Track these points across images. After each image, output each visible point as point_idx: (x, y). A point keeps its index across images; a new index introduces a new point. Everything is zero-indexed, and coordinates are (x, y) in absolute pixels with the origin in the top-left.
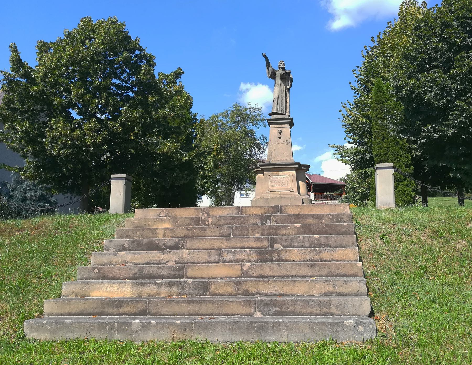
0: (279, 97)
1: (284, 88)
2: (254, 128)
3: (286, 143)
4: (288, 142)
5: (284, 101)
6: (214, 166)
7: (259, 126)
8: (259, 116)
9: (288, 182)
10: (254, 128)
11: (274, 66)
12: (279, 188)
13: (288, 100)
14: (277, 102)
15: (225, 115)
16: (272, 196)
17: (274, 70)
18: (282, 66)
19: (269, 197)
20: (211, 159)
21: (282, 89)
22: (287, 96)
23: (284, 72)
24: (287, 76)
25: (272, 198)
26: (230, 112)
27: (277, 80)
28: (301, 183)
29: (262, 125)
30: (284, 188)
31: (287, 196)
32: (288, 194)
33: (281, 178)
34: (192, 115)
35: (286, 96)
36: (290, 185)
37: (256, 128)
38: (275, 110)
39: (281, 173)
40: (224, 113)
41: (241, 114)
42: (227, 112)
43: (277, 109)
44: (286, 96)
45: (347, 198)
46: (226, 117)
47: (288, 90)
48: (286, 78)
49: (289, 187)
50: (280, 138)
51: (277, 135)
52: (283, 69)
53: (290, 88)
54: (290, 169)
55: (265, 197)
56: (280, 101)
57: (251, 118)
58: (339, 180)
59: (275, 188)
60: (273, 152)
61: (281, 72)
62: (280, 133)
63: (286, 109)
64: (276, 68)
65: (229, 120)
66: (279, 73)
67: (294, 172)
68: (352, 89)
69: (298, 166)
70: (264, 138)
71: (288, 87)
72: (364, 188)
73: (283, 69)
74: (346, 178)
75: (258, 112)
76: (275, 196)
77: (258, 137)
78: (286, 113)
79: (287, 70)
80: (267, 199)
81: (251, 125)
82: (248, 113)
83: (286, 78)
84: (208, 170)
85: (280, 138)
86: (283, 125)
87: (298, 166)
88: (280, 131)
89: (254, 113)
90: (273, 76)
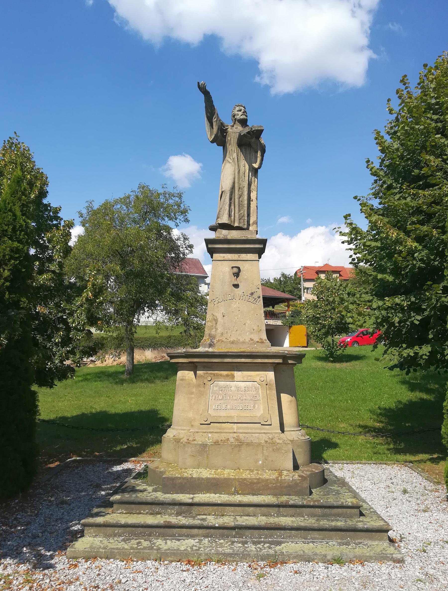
0: (233, 188)
1: (245, 166)
2: (171, 224)
3: (251, 299)
4: (255, 296)
5: (246, 198)
6: (88, 318)
7: (178, 221)
8: (179, 206)
9: (255, 400)
10: (171, 224)
11: (224, 114)
12: (235, 415)
13: (253, 195)
14: (231, 199)
15: (125, 201)
16: (216, 437)
17: (222, 124)
18: (240, 116)
19: (209, 439)
20: (82, 305)
21: (242, 169)
22: (253, 187)
23: (247, 130)
24: (253, 140)
25: (216, 443)
26: (132, 198)
27: (229, 148)
28: (285, 397)
29: (183, 219)
30: (246, 415)
31: (254, 438)
32: (257, 435)
33: (238, 389)
34: (50, 211)
35: (250, 185)
36: (262, 407)
37: (174, 223)
38: (225, 219)
39: (237, 374)
40: (124, 198)
41: (151, 202)
42: (128, 197)
43: (230, 216)
44: (250, 185)
45: (292, 316)
46: (127, 205)
47: (255, 172)
48: (251, 143)
49: (259, 414)
50: (236, 286)
51: (229, 278)
52: (244, 122)
53: (260, 167)
54: (263, 367)
55: (200, 439)
56: (237, 197)
57: (165, 209)
58: (272, 282)
59: (223, 414)
60: (220, 320)
61: (239, 128)
62: (237, 275)
63: (249, 215)
64: (228, 122)
65: (132, 210)
66: (234, 132)
67: (271, 375)
68: (372, 174)
69: (280, 361)
70: (185, 239)
71: (256, 166)
72: (332, 318)
73: (244, 122)
74: (282, 279)
75: (177, 199)
76: (223, 437)
77: (176, 237)
78: (249, 225)
79: (253, 124)
80: (204, 446)
81: (166, 219)
82: (162, 200)
83: (251, 143)
84: (76, 328)
85: (236, 286)
86: (244, 256)
87: (280, 361)
88: (236, 270)
89: (171, 201)
90: (220, 139)
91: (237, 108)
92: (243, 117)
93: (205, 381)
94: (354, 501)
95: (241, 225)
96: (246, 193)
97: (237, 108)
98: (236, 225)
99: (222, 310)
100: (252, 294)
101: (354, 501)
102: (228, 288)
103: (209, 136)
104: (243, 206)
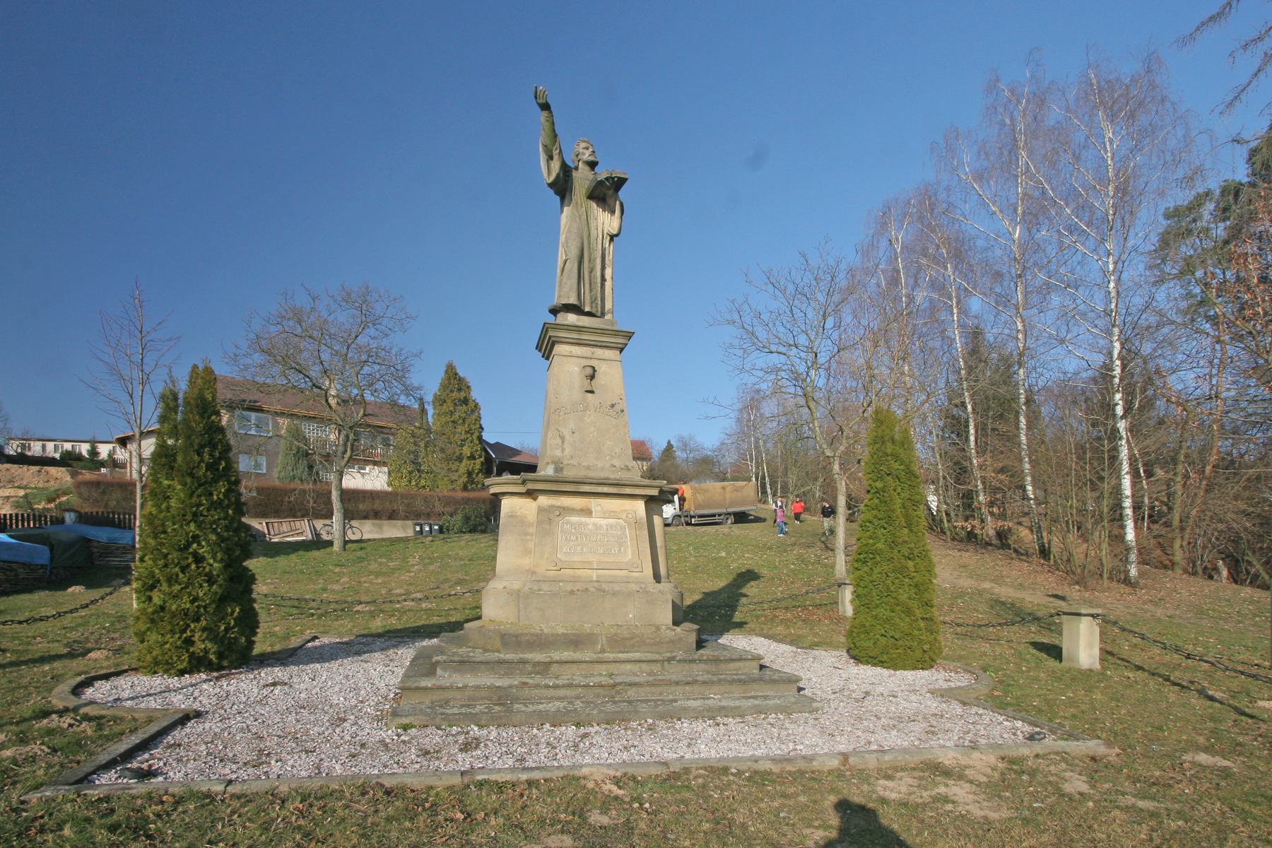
5: (599, 274)
33: (597, 527)
36: (630, 551)
62: (592, 377)
86: (599, 352)
88: (589, 371)
91: (583, 145)
92: (592, 158)
93: (551, 516)
94: (135, 765)
95: (594, 311)
96: (599, 267)
97: (583, 145)
98: (587, 309)
99: (572, 425)
100: (613, 406)
101: (135, 765)
102: (577, 394)
103: (545, 175)
104: (595, 277)
